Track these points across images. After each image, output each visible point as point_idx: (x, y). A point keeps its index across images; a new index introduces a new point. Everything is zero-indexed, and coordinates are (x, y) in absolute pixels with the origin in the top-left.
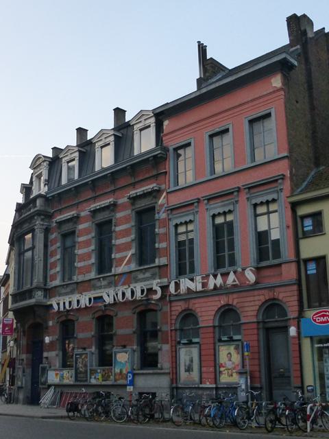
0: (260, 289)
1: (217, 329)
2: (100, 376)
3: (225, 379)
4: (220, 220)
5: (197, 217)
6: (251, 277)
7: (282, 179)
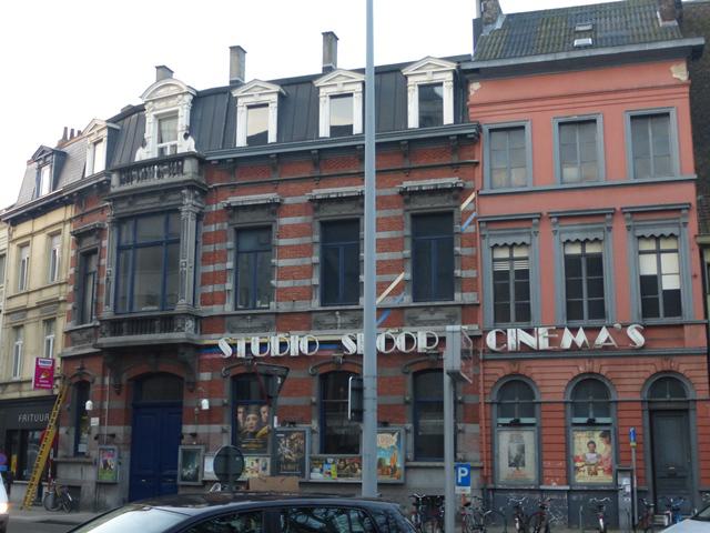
0: (649, 356)
1: (569, 407)
2: (333, 468)
3: (583, 478)
4: (575, 250)
5: (536, 241)
6: (637, 337)
7: (539, 219)
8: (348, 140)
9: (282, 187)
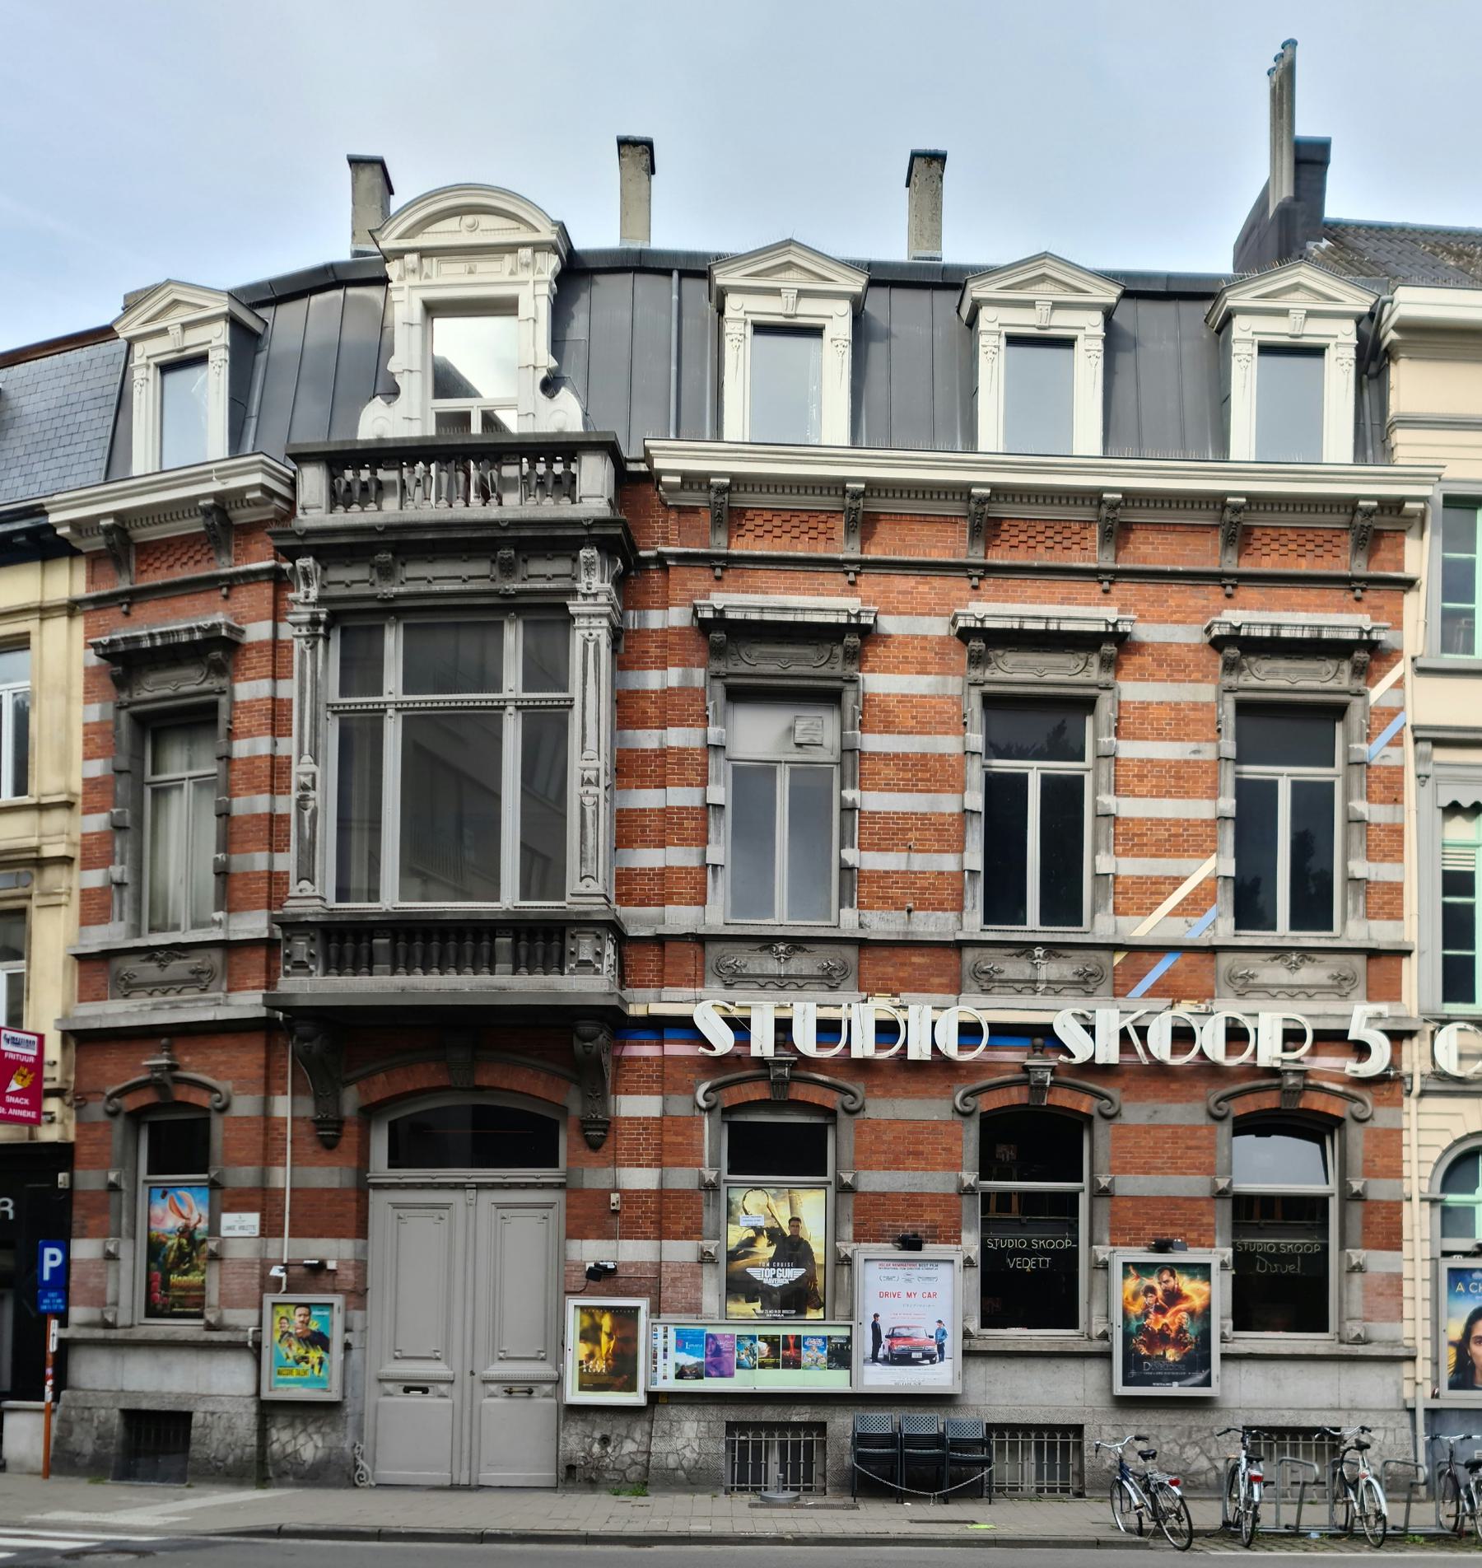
8: (1216, 474)
9: (870, 583)
